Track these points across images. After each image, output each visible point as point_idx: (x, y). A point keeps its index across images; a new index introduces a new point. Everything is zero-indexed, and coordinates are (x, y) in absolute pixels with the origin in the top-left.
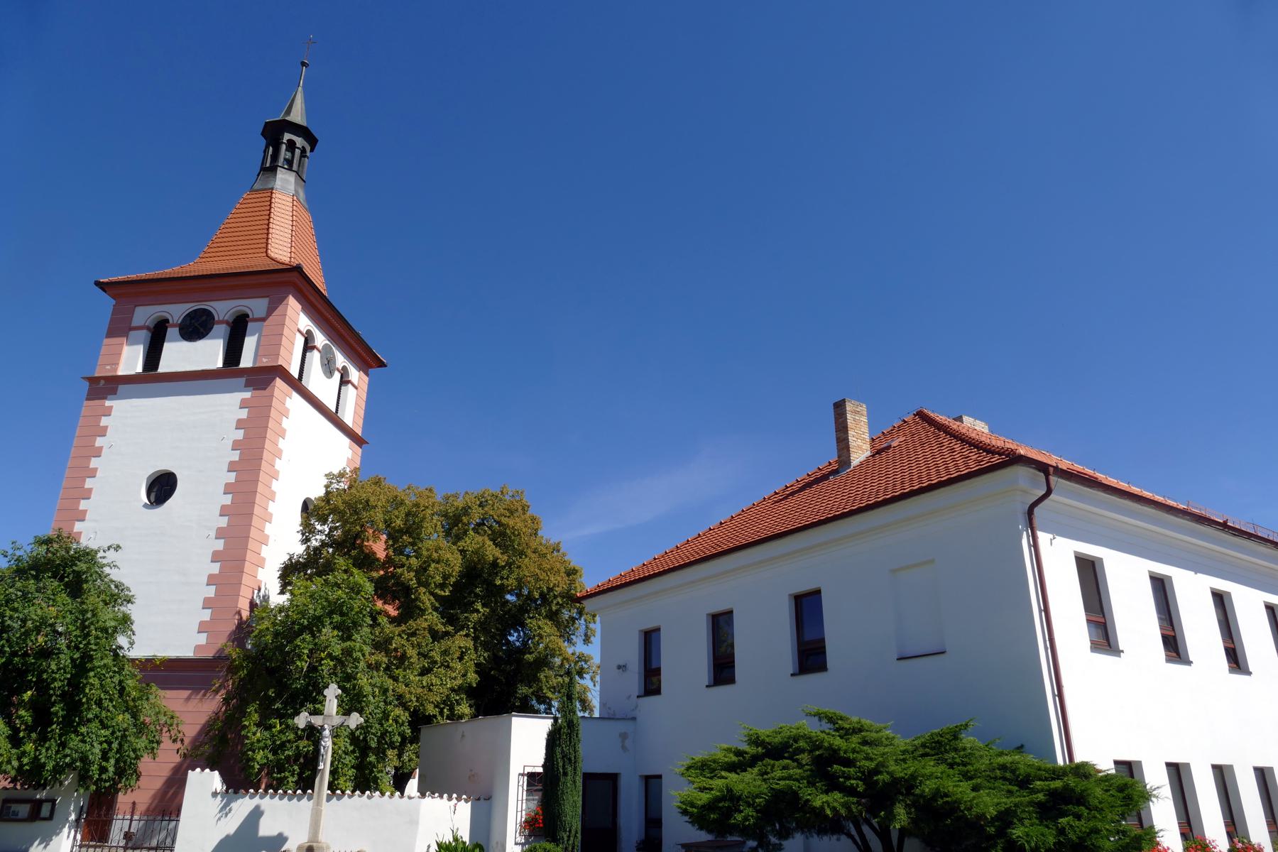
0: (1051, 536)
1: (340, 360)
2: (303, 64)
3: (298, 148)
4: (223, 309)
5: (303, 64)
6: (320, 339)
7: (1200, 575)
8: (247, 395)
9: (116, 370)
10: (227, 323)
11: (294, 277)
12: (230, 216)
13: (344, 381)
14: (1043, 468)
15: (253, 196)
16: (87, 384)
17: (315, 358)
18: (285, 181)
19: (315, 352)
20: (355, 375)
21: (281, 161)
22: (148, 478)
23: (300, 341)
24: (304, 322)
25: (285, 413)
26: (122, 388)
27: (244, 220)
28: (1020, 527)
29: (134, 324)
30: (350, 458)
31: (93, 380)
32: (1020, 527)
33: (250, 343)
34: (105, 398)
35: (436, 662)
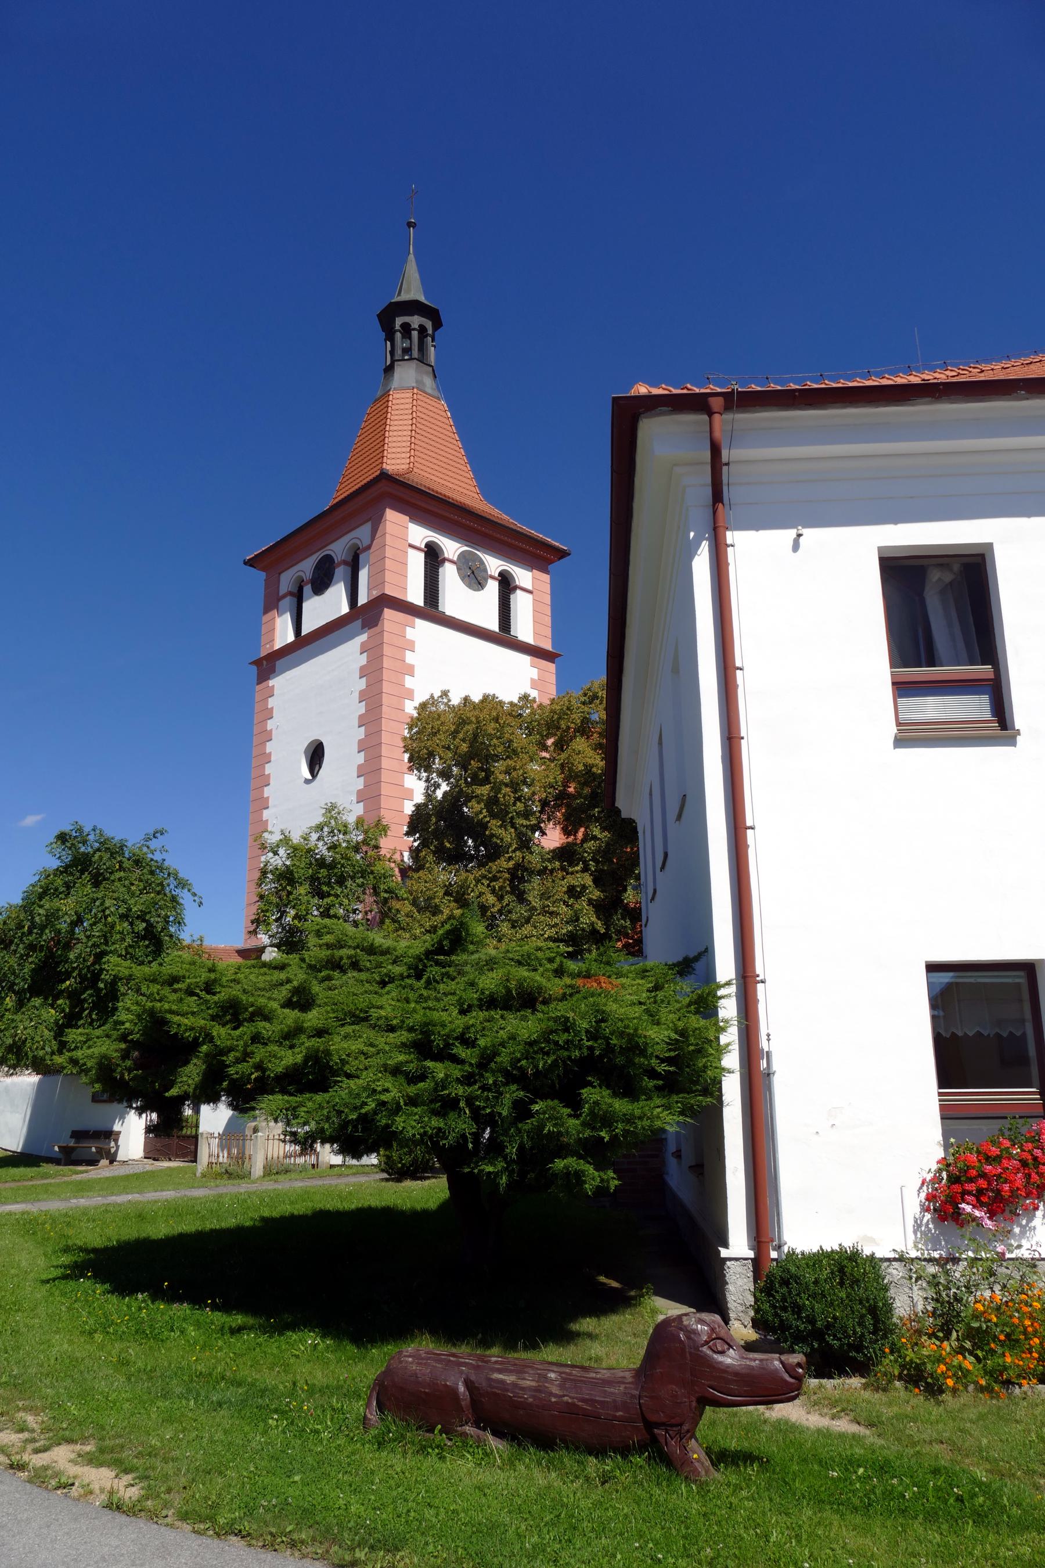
0: (792, 533)
1: (494, 564)
2: (410, 225)
3: (414, 329)
4: (338, 549)
5: (410, 225)
6: (451, 548)
7: (761, 532)
8: (364, 637)
9: (273, 646)
10: (345, 563)
11: (383, 487)
12: (357, 439)
13: (507, 585)
14: (697, 404)
15: (378, 405)
16: (254, 668)
17: (449, 575)
18: (406, 374)
19: (447, 565)
20: (523, 576)
21: (399, 352)
22: (306, 752)
23: (416, 563)
24: (419, 534)
25: (411, 646)
26: (279, 664)
27: (367, 439)
28: (692, 534)
29: (281, 593)
30: (536, 677)
31: (258, 663)
32: (692, 534)
33: (363, 575)
34: (269, 679)
35: (534, 909)
